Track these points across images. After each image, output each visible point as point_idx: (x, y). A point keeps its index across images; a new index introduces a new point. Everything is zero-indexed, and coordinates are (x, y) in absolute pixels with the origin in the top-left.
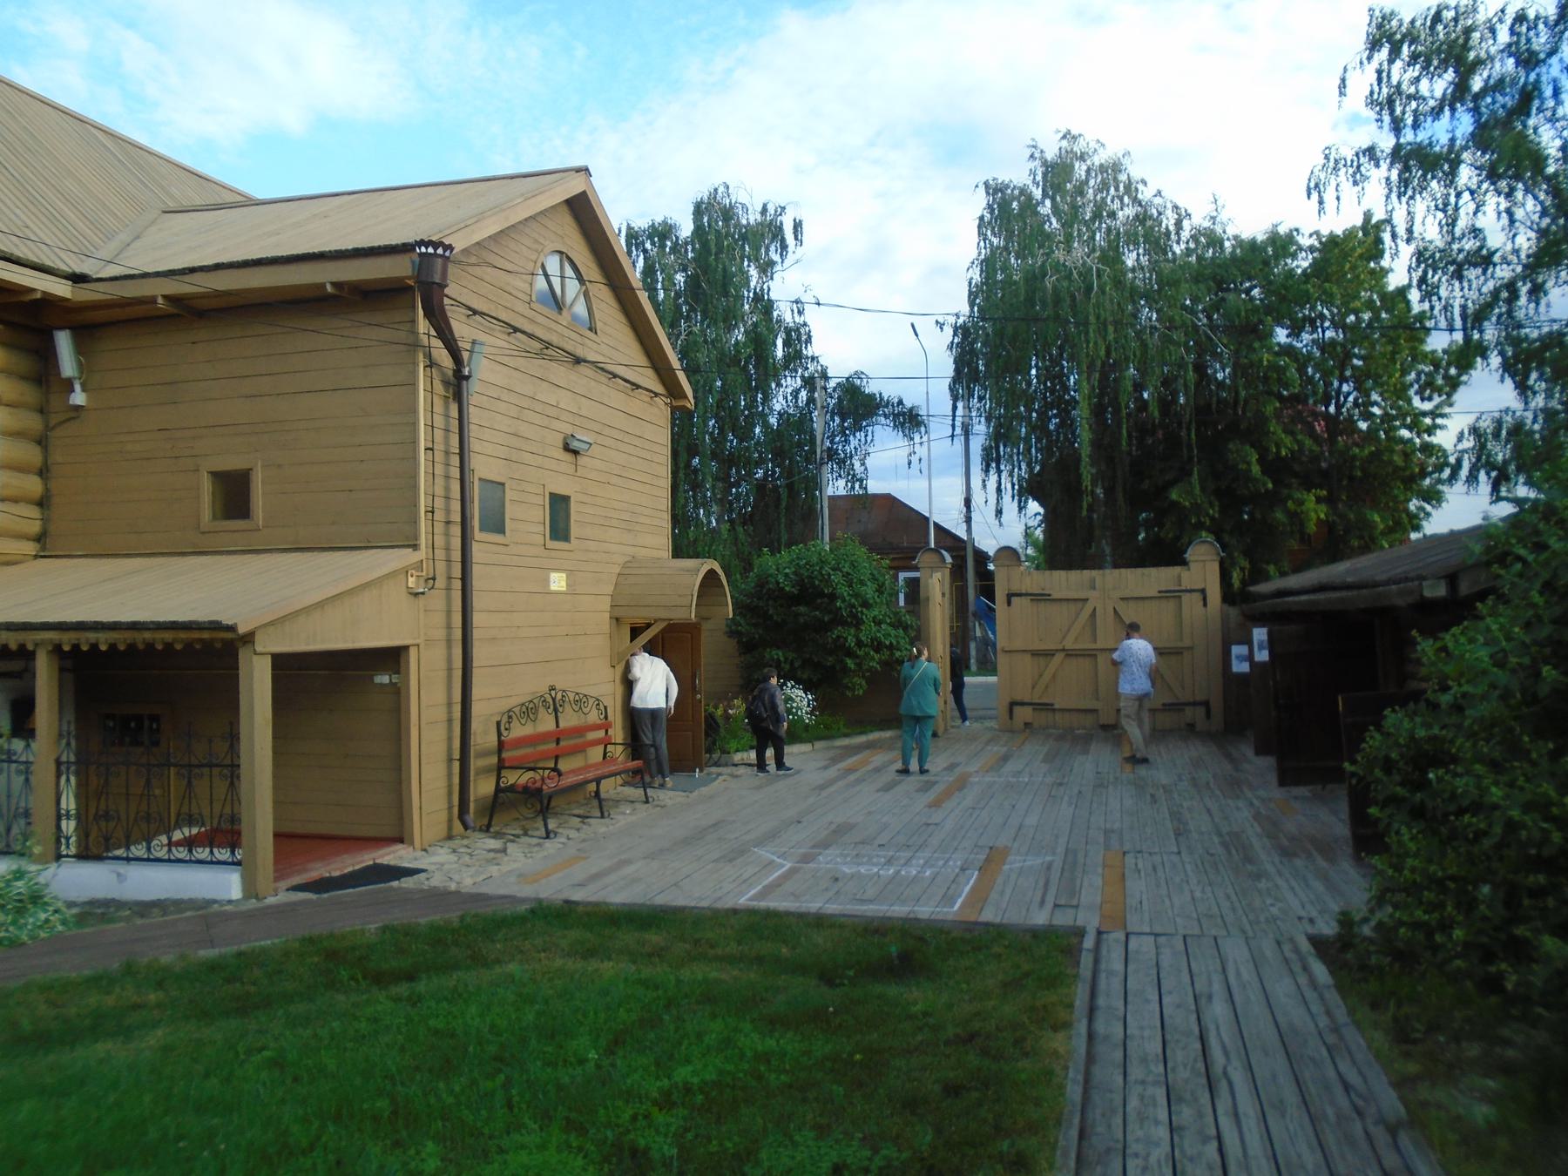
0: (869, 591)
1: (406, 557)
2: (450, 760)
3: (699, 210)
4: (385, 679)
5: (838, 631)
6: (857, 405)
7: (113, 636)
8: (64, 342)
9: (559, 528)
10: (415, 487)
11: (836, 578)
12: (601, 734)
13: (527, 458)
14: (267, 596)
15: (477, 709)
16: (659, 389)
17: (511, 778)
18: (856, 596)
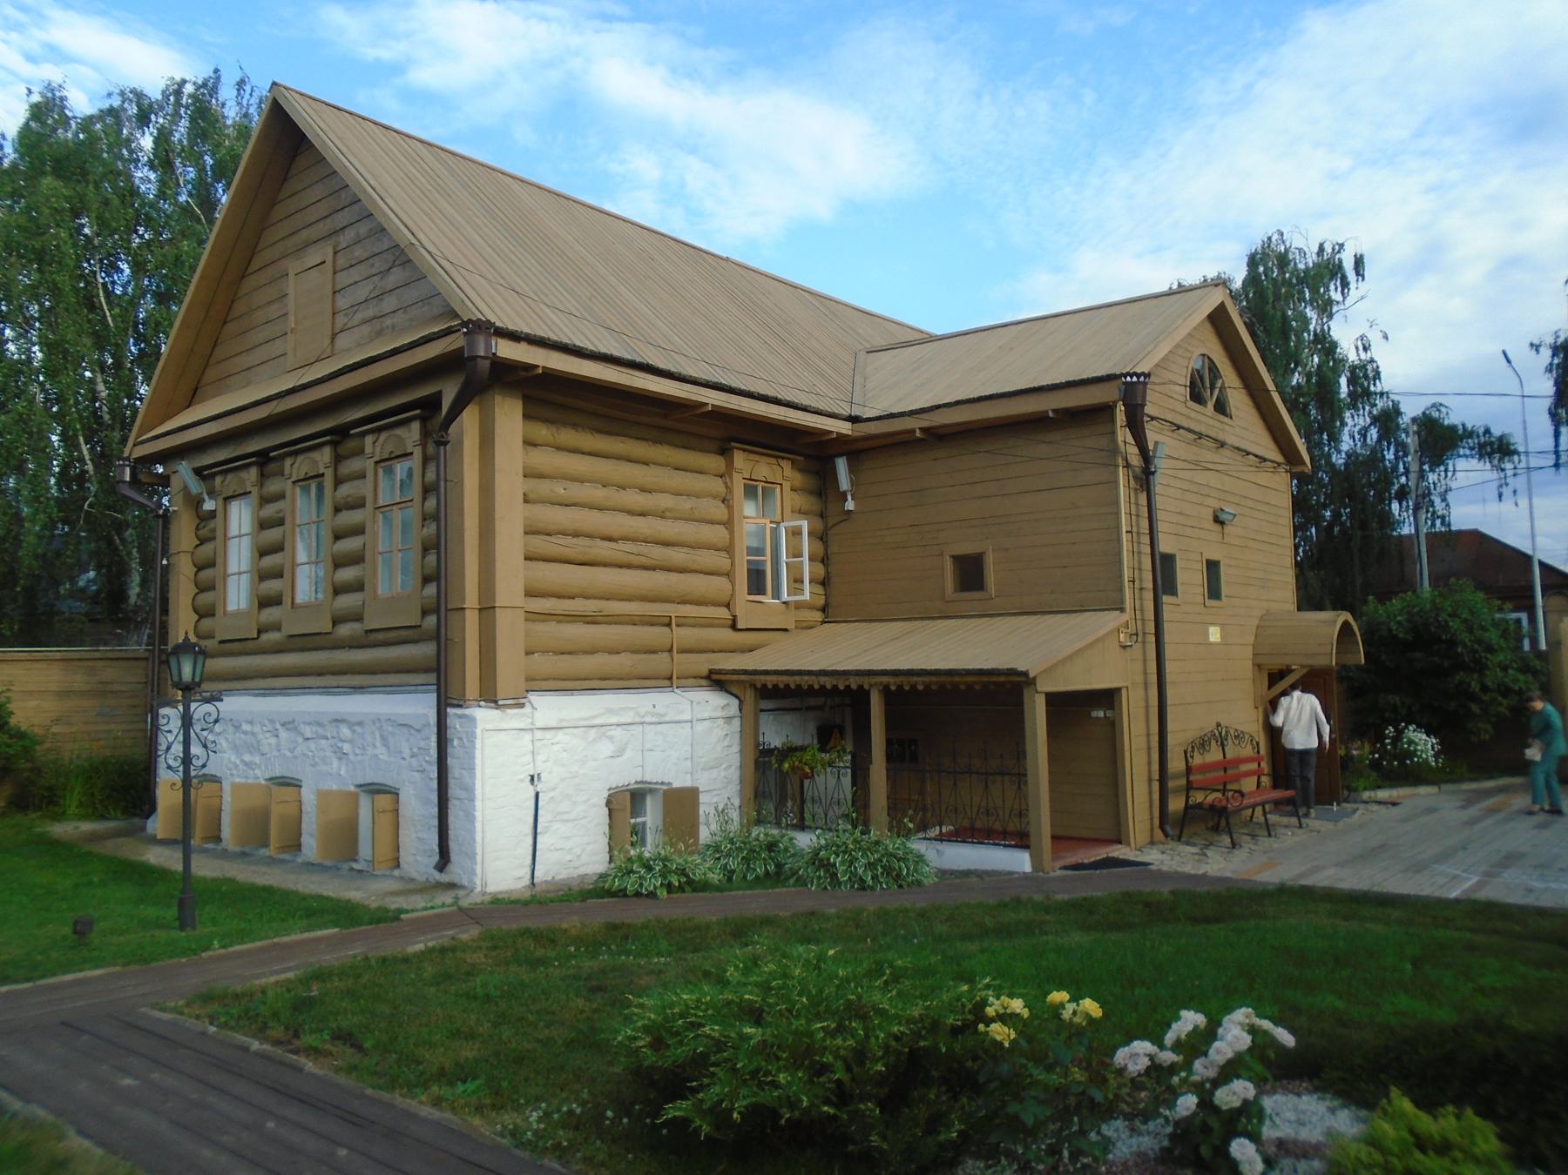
0: (1493, 636)
1: (1112, 620)
2: (1150, 780)
3: (1253, 261)
4: (1101, 714)
5: (1460, 676)
6: (1440, 439)
7: (774, 678)
8: (842, 465)
9: (1214, 592)
10: (1120, 562)
11: (1454, 624)
12: (1254, 766)
13: (1189, 532)
14: (1055, 649)
15: (1171, 740)
16: (1279, 458)
17: (1198, 797)
18: (1479, 641)
